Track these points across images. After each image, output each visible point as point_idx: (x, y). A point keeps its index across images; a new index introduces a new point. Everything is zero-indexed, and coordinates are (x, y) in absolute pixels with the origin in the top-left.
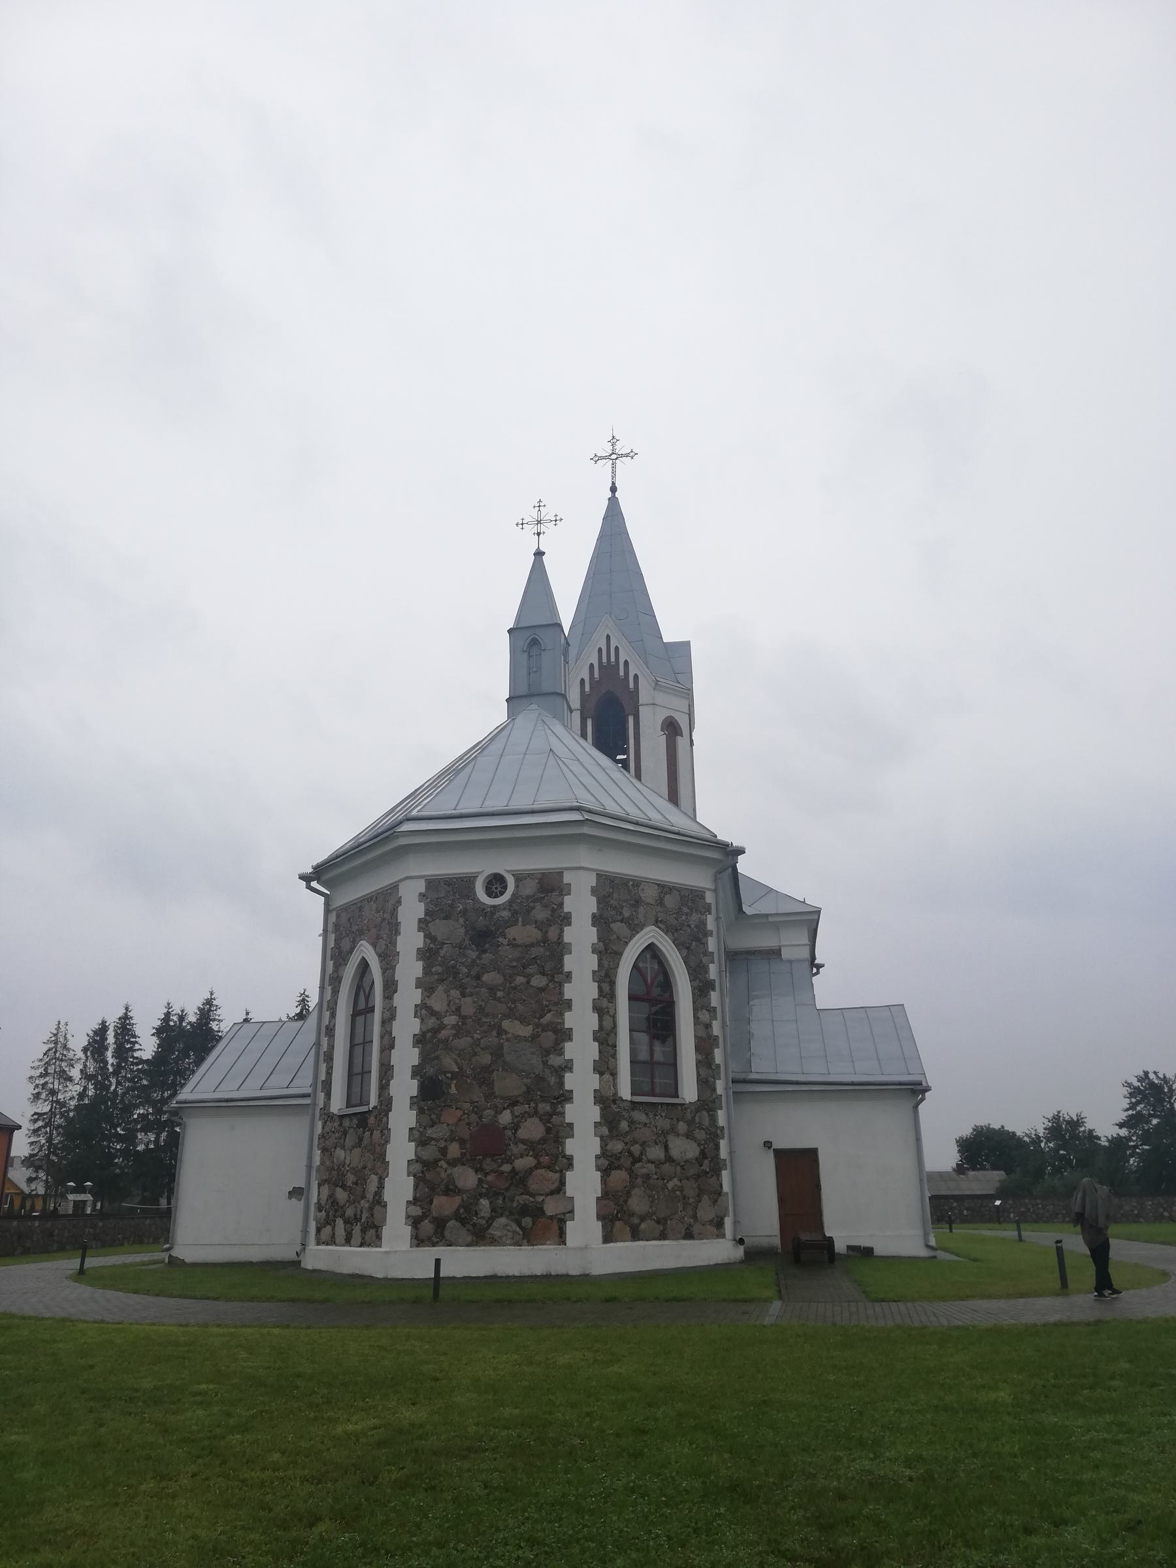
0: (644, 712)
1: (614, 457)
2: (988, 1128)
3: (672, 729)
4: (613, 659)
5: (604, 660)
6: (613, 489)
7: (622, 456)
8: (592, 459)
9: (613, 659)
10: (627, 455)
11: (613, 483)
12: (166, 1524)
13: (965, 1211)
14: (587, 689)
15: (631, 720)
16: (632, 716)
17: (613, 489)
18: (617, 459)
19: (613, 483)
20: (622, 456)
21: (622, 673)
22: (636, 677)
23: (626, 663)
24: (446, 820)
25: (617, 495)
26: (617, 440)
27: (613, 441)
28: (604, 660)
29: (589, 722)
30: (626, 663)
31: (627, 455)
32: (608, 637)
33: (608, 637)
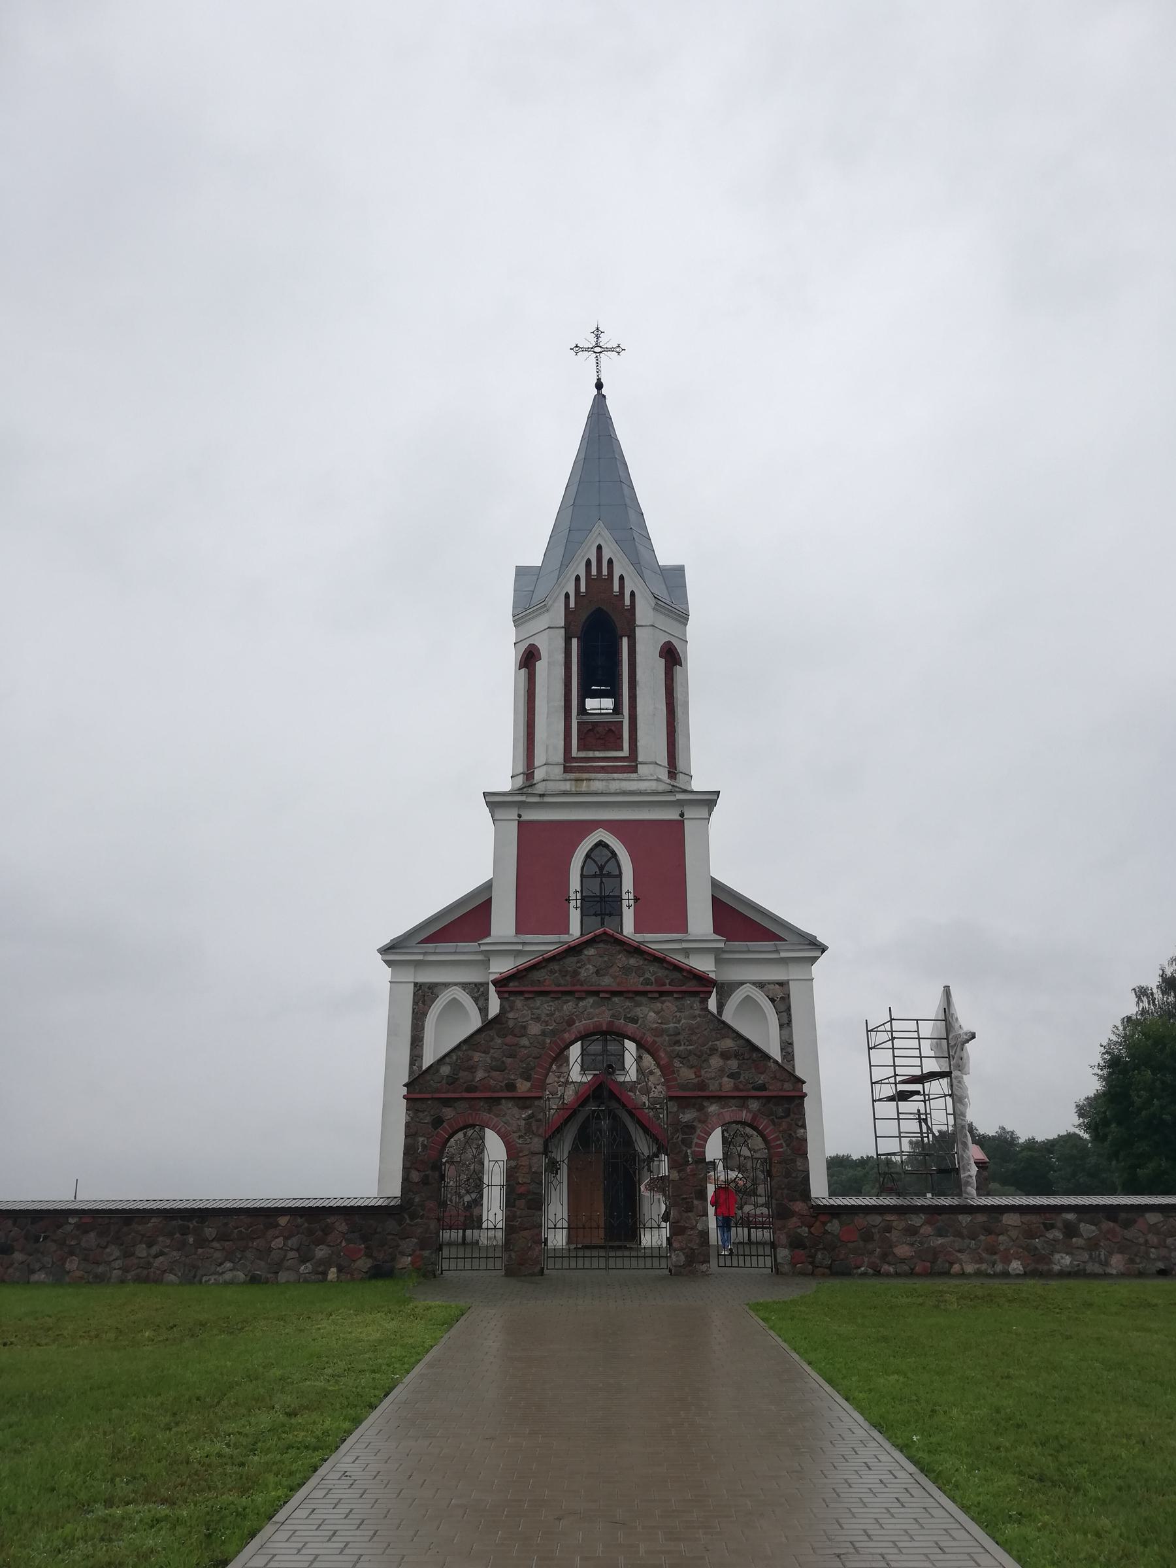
0: (639, 633)
1: (598, 349)
2: (848, 1157)
3: (672, 657)
4: (605, 572)
5: (594, 571)
6: (599, 385)
7: (587, 350)
8: (572, 349)
9: (605, 572)
10: (612, 350)
11: (599, 379)
12: (874, 1414)
13: (259, 1304)
14: (572, 604)
15: (625, 641)
16: (576, 639)
17: (599, 385)
18: (600, 352)
19: (599, 379)
20: (587, 350)
21: (616, 588)
22: (632, 594)
23: (621, 578)
24: (680, 728)
25: (604, 391)
26: (593, 332)
27: (598, 333)
28: (594, 571)
29: (575, 641)
30: (621, 578)
31: (612, 350)
32: (599, 548)
33: (599, 548)
